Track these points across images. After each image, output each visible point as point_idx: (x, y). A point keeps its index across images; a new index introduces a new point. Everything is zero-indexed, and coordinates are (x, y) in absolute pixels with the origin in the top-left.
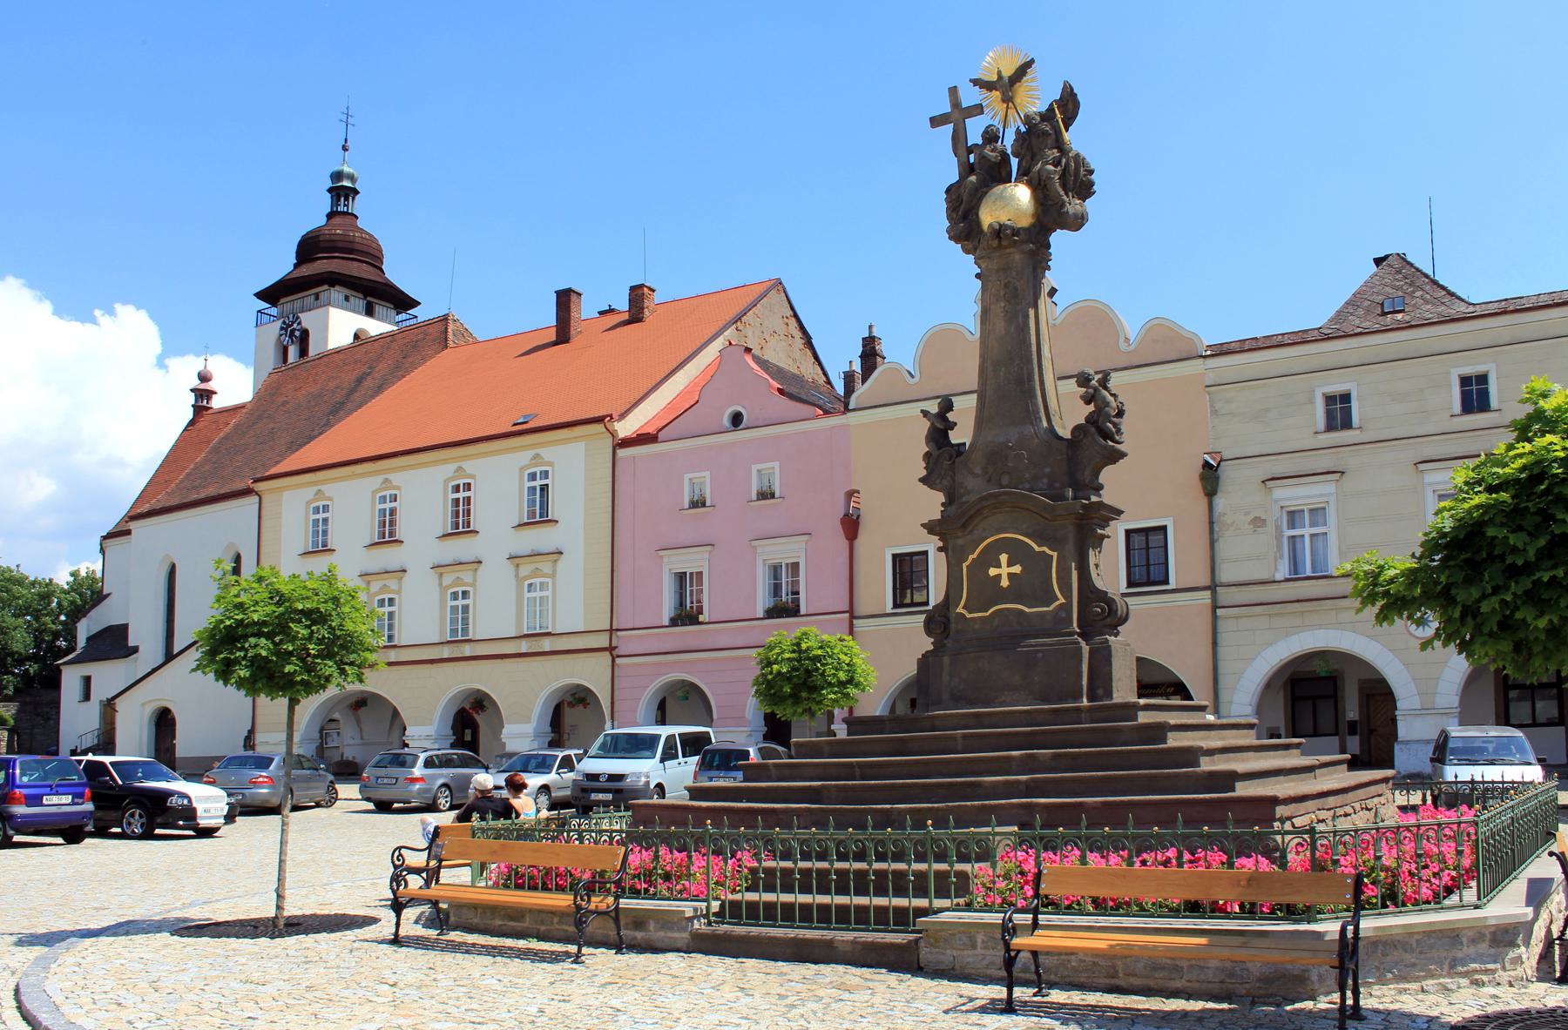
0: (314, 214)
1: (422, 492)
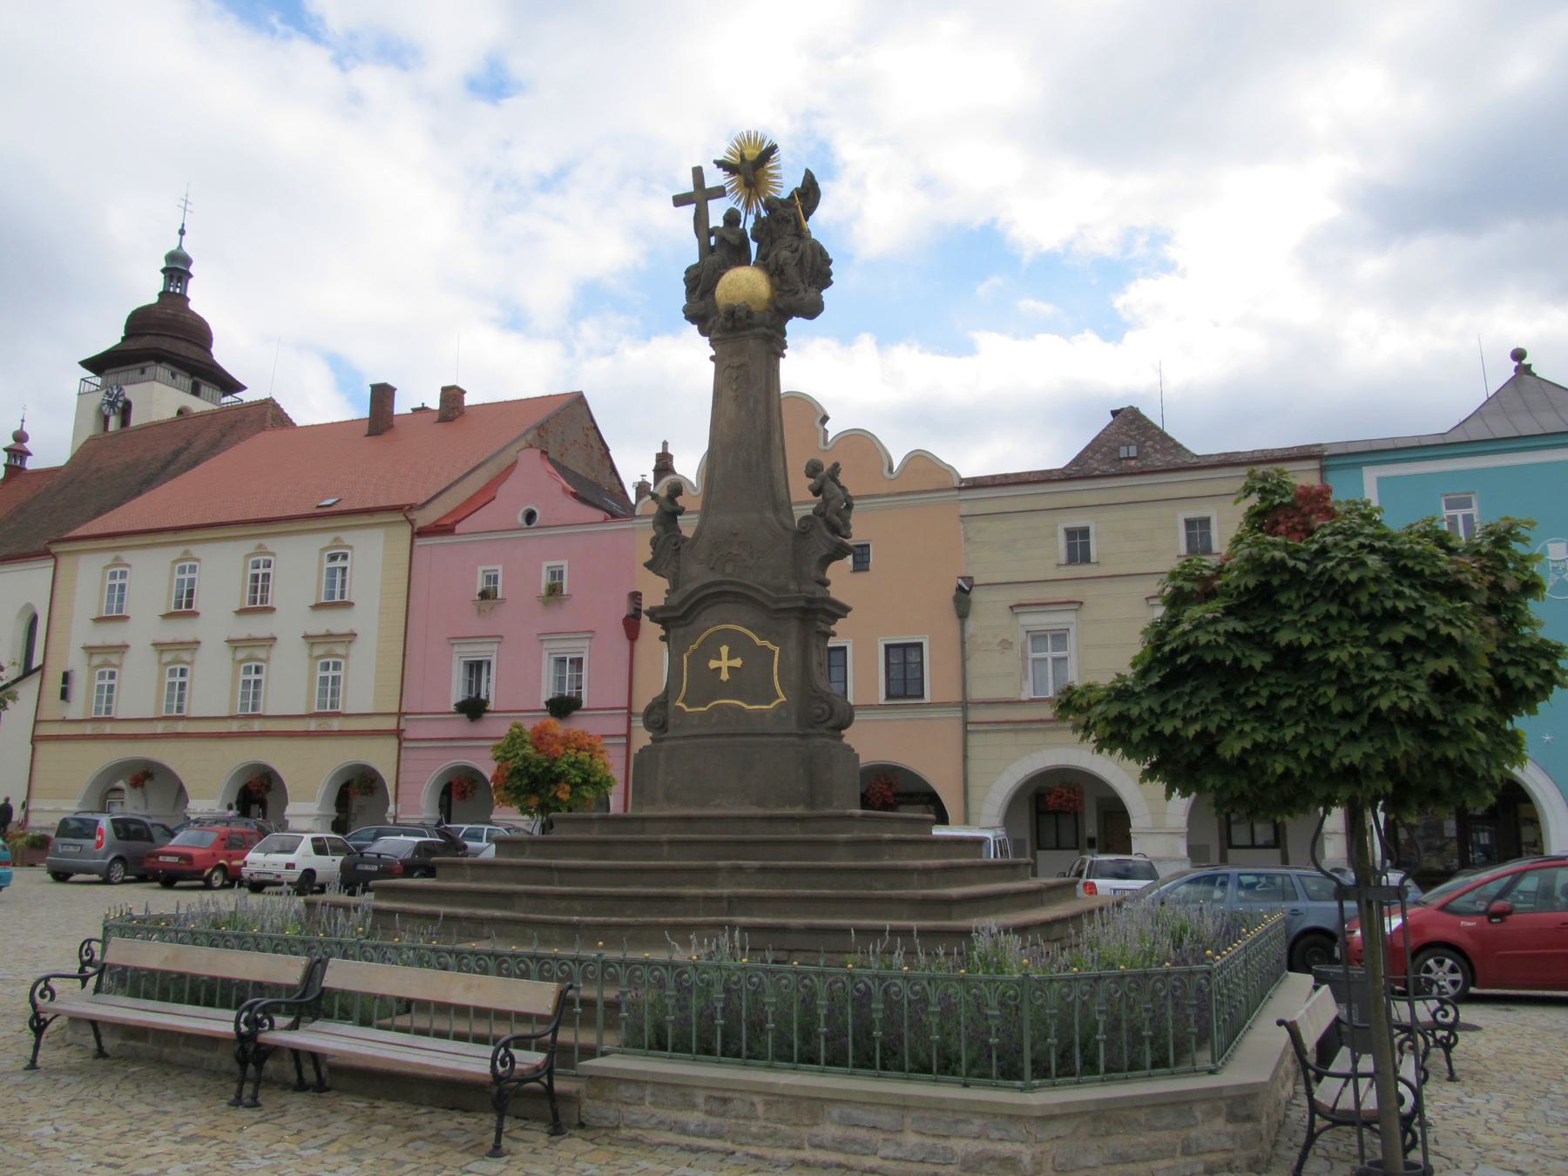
0: (148, 289)
1: (222, 569)
